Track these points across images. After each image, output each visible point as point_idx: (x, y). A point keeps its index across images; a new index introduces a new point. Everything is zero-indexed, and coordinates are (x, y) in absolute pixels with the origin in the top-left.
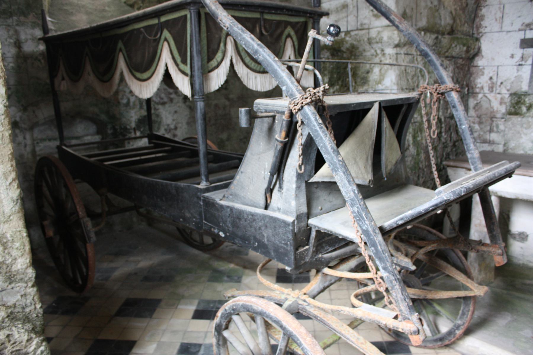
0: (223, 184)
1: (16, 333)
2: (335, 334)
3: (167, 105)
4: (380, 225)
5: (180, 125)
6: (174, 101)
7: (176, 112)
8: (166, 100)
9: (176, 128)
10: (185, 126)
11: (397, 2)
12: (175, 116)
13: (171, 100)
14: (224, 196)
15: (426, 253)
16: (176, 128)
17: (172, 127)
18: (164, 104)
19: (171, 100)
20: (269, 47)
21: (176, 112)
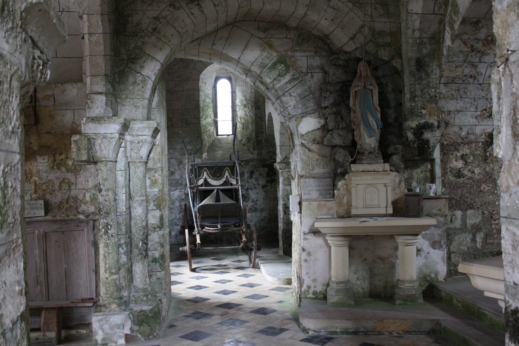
0: (230, 248)
1: (100, 196)
2: (144, 78)
3: (253, 190)
4: (271, 112)
5: (259, 199)
6: (257, 188)
7: (257, 193)
8: (253, 187)
9: (257, 201)
10: (262, 200)
11: (503, 343)
12: (257, 195)
13: (256, 188)
14: (325, 298)
15: (25, 160)
16: (257, 201)
17: (255, 200)
18: (251, 189)
19: (256, 188)
20: (274, 135)
21: (257, 193)
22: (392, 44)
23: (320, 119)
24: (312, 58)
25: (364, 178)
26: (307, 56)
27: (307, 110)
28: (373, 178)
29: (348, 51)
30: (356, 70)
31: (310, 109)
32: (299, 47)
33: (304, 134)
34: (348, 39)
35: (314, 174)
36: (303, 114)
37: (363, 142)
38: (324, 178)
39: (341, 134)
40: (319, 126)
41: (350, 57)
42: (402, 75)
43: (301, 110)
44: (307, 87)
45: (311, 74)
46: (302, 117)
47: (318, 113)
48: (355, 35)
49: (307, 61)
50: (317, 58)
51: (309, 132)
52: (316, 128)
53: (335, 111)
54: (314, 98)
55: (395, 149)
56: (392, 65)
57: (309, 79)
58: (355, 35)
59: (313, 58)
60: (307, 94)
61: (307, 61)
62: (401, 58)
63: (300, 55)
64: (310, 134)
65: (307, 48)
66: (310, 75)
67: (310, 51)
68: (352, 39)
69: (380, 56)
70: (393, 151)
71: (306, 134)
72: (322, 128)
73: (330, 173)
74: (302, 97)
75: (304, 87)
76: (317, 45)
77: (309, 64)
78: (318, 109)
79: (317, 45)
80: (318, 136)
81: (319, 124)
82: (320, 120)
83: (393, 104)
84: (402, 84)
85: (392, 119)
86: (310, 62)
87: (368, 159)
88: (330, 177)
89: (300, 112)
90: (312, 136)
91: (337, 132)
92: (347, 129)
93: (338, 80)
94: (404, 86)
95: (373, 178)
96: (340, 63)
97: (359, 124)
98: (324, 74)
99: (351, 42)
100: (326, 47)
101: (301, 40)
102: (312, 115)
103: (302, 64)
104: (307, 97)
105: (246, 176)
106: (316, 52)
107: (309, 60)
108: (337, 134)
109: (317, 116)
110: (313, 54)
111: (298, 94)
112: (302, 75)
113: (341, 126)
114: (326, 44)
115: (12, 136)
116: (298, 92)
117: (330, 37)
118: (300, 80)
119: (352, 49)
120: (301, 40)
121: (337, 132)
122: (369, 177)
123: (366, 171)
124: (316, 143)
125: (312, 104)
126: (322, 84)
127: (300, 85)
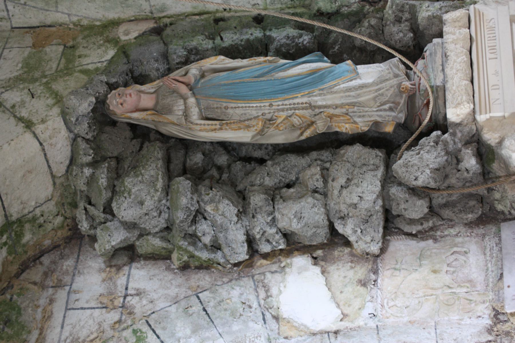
22: (71, 44)
23: (287, 270)
24: (73, 297)
25: (493, 80)
26: (67, 309)
27: (255, 305)
28: (493, 56)
29: (69, 148)
30: (133, 127)
31: (252, 297)
32: (30, 332)
33: (339, 312)
34: (28, 136)
35: (486, 279)
36: (268, 316)
37: (374, 99)
38: (501, 250)
39: (342, 181)
40: (317, 270)
41: (87, 141)
42: (167, 21)
43: (251, 324)
44: (173, 309)
45: (129, 298)
46: (276, 318)
47: (269, 275)
48: (21, 119)
49: (82, 308)
50: (79, 282)
51: (333, 297)
52: (321, 279)
53: (263, 196)
54: (212, 288)
55: (398, 20)
56: (133, 41)
57: (144, 302)
58: (21, 119)
59: (75, 292)
60: (197, 308)
61: (82, 308)
62: (115, 23)
63: (58, 329)
64: (341, 297)
65: (40, 310)
66: (132, 301)
67: (52, 301)
68: (29, 125)
69: (99, 65)
70: (405, 26)
71: (338, 306)
72: (323, 263)
73: (484, 236)
74: (204, 321)
75: (173, 316)
76: (35, 283)
77: (93, 304)
78: (253, 277)
79: (35, 283)
80: (351, 274)
81: (306, 269)
82: (294, 268)
83: (257, 33)
84: (197, 17)
85: (301, 36)
86: (87, 302)
87: (430, 70)
88: (498, 234)
89: (258, 327)
90: (349, 289)
91: (336, 192)
92: (328, 165)
93: (160, 184)
94: (200, 14)
95: (493, 56)
96: (103, 181)
97: (311, 106)
98: (134, 265)
99: (39, 129)
100: (46, 260)
101: (6, 330)
102: (274, 291)
103: (91, 322)
104: (209, 310)
105: (452, 223)
106: (59, 285)
107: (79, 305)
108: (345, 192)
109: (278, 277)
110: (62, 295)
111: (194, 331)
112: (129, 322)
113: (320, 184)
114: (37, 259)
115: (47, 69)
116: (188, 332)
117: (15, 217)
118: (145, 328)
119: (64, 132)
120: (6, 330)
121: (336, 192)
122: (492, 66)
123: (469, 71)
124: (373, 277)
125: (235, 293)
126: (168, 268)
127: (164, 329)
